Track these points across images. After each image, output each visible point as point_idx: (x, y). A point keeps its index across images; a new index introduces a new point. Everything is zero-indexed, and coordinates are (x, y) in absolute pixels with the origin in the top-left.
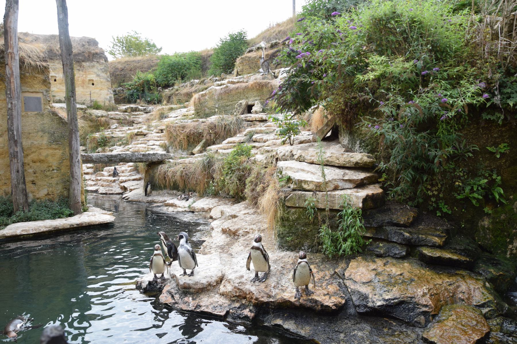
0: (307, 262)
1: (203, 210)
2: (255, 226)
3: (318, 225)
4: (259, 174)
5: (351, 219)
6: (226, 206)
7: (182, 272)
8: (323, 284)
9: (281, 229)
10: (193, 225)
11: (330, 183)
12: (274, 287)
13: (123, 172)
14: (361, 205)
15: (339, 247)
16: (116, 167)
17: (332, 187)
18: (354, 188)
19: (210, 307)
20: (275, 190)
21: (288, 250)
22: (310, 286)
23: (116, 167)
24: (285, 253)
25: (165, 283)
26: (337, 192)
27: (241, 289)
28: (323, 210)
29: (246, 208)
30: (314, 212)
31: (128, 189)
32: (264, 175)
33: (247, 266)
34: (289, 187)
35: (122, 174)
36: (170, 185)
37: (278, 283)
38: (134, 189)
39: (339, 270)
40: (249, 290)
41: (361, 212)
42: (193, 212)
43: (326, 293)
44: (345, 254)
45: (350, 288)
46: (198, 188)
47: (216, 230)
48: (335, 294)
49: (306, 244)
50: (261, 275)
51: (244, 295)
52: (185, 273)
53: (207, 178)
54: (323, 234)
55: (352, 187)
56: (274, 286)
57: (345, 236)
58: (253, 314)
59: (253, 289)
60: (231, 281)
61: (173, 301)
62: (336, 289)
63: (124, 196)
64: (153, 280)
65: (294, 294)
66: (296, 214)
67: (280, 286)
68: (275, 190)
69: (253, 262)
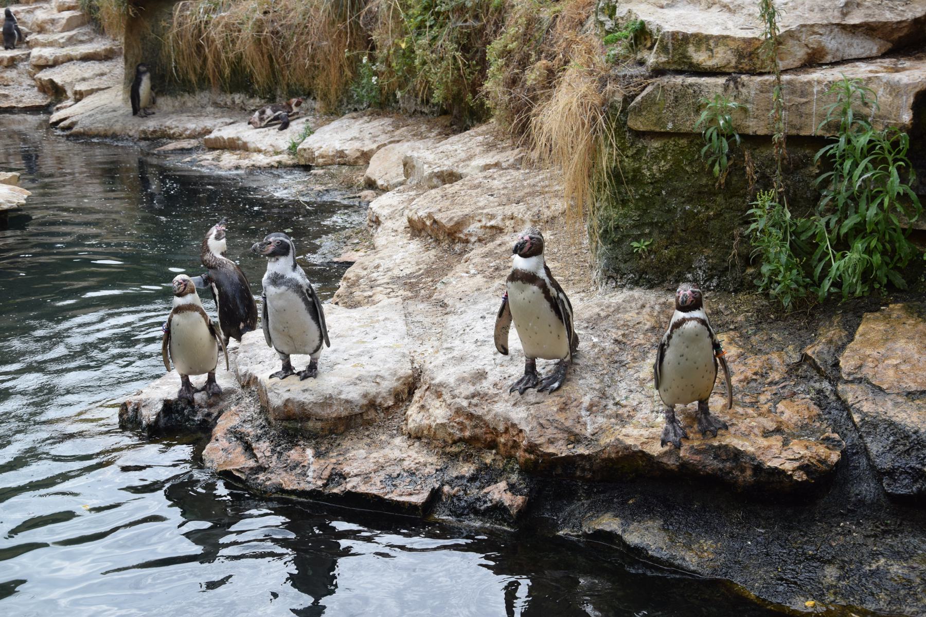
0: (703, 322)
1: (341, 159)
2: (522, 207)
3: (744, 196)
4: (532, 22)
5: (866, 169)
6: (419, 144)
7: (278, 366)
8: (762, 398)
9: (613, 214)
10: (309, 213)
11: (791, 42)
12: (590, 409)
13: (41, 29)
14: (907, 117)
15: (819, 270)
16: (13, 9)
17: (801, 53)
18: (884, 56)
19: (377, 479)
20: (591, 73)
21: (636, 283)
22: (716, 403)
23: (13, 9)
24: (626, 294)
25: (223, 404)
26: (817, 75)
27: (479, 418)
28: (766, 140)
29: (490, 147)
30: (731, 150)
31: (69, 93)
32: (553, 25)
33: (496, 338)
34: (641, 63)
35: (41, 37)
36: (221, 73)
37: (603, 395)
38: (91, 92)
39: (818, 348)
40: (507, 419)
41: (904, 144)
42: (307, 168)
43: (771, 426)
44: (840, 296)
45: (859, 411)
46: (320, 83)
47: (388, 224)
48: (804, 430)
49: (702, 260)
50: (544, 367)
51: (489, 437)
52: (288, 368)
53: (352, 47)
54: (761, 224)
55: (875, 52)
56: (592, 406)
57: (844, 230)
58: (519, 500)
59: (518, 415)
60: (444, 391)
61: (252, 463)
62: (806, 414)
63: (55, 117)
64: (180, 397)
65: (659, 431)
66: (664, 157)
67: (610, 403)
68: (591, 73)
69: (518, 326)
